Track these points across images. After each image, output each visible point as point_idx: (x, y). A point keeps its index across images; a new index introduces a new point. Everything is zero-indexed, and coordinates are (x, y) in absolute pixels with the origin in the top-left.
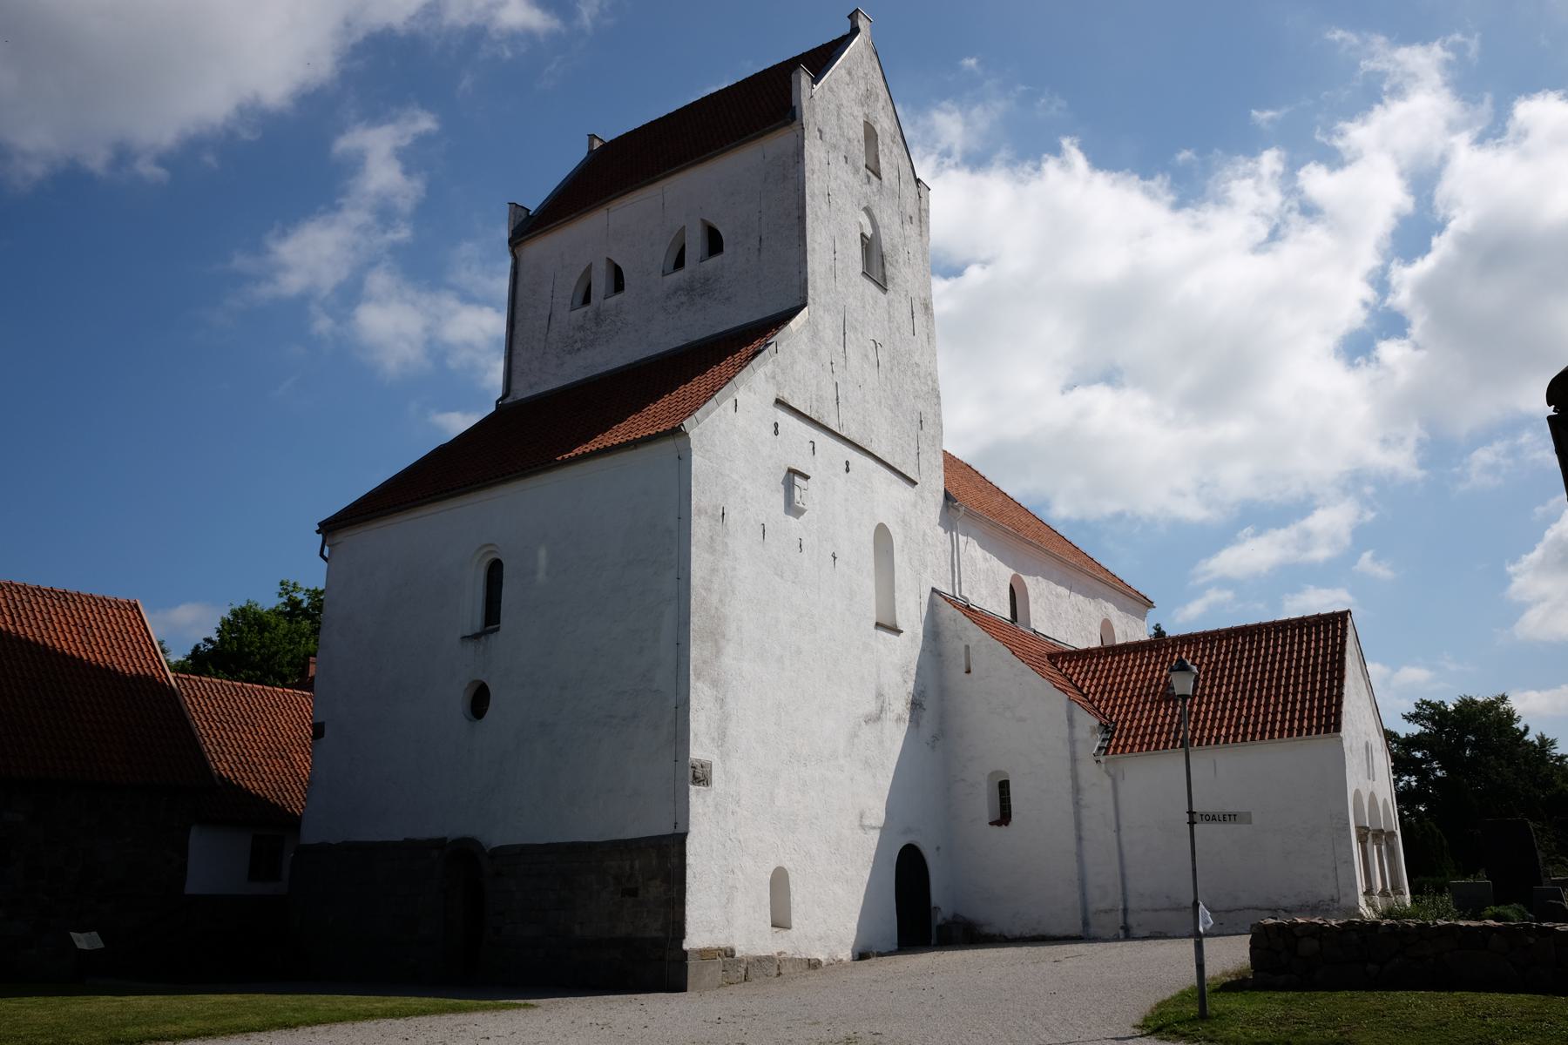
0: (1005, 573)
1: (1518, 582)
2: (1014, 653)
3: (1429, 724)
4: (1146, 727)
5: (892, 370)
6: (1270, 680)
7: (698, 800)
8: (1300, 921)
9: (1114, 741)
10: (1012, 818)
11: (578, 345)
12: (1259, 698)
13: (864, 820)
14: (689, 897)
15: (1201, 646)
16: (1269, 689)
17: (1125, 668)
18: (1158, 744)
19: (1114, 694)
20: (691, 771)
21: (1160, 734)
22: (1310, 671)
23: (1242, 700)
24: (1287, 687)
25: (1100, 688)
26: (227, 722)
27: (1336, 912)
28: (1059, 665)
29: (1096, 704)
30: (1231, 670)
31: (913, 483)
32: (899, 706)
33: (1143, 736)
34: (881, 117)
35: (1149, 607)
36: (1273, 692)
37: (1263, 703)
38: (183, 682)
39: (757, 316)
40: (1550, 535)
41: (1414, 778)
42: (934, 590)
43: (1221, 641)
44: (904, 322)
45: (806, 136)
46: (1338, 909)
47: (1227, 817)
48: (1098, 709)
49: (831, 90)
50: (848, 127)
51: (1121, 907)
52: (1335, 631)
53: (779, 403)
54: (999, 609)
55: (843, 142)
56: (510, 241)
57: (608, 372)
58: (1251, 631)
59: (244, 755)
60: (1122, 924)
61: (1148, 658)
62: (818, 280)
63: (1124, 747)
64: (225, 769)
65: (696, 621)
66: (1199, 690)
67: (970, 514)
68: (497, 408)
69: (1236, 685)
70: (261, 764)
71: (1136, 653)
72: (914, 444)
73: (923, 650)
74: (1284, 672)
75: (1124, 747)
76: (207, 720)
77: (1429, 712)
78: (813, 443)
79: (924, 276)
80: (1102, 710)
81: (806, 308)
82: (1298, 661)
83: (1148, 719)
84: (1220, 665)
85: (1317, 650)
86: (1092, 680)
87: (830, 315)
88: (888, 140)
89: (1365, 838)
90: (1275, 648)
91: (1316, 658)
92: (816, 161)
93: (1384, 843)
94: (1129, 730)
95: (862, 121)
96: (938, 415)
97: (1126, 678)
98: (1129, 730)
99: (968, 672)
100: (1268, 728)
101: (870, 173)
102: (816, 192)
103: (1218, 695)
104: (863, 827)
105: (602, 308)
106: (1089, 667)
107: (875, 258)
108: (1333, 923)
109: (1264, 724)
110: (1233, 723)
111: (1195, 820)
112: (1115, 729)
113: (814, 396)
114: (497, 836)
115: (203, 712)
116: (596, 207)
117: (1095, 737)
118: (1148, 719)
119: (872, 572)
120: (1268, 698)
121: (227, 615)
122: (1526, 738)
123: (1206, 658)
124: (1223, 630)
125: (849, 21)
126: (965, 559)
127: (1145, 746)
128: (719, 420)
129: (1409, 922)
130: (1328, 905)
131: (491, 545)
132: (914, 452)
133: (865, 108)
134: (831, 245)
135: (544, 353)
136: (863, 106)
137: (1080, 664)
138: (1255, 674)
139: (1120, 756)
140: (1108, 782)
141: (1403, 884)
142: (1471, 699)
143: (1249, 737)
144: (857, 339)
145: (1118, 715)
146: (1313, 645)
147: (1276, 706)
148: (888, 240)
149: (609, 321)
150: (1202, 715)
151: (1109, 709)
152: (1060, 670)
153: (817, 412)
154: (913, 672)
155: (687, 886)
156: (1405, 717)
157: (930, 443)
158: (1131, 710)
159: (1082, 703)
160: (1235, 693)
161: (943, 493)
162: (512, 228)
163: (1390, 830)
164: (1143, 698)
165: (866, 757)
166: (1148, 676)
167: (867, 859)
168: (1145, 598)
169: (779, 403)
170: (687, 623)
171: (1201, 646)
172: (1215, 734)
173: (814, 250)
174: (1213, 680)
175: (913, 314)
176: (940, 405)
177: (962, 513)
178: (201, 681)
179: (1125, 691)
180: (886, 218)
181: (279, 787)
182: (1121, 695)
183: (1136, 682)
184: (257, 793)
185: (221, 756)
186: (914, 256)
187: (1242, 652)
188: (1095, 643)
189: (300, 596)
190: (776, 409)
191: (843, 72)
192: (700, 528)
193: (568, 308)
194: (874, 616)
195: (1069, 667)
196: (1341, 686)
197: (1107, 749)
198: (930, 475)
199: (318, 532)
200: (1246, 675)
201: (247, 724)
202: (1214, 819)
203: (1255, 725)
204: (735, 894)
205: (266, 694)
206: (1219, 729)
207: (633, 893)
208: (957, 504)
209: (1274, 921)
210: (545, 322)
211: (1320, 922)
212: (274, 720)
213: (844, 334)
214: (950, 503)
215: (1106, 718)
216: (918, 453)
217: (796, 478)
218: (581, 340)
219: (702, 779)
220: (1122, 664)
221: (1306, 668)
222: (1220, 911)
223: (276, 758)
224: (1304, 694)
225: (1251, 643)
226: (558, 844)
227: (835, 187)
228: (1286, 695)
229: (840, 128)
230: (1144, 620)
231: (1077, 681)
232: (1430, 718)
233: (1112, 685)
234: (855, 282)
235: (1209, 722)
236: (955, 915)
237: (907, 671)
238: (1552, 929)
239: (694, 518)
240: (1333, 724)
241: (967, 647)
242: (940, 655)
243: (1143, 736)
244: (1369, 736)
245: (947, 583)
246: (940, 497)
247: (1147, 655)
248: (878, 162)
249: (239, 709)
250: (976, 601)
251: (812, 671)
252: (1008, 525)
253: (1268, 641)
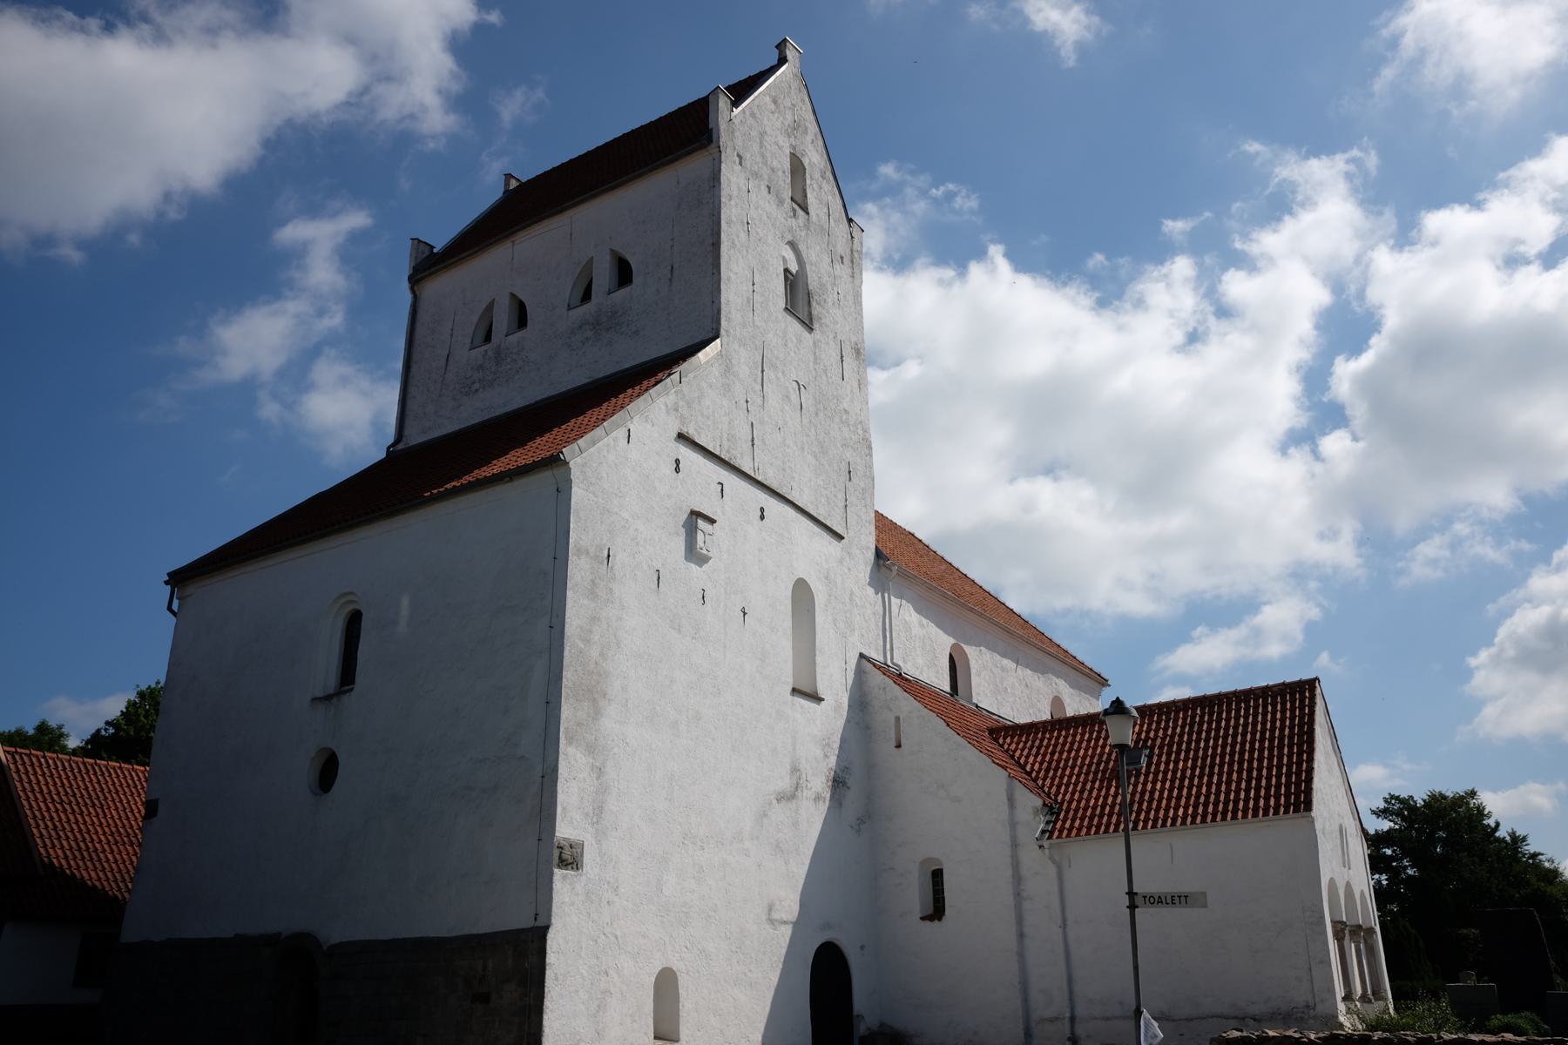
0: (945, 642)
1: (1479, 678)
2: (948, 725)
3: (1399, 820)
4: (1094, 808)
5: (817, 414)
6: (1232, 755)
7: (561, 880)
8: (1271, 1033)
9: (1060, 823)
10: (946, 913)
11: (477, 386)
12: (1220, 774)
13: (773, 913)
14: (548, 1003)
15: (1155, 719)
16: (1231, 764)
17: (1072, 744)
18: (1108, 826)
19: (1060, 771)
20: (556, 853)
21: (1110, 815)
22: (1276, 744)
23: (1201, 777)
24: (1250, 762)
25: (1045, 764)
26: (70, 803)
27: (1312, 1021)
28: (1001, 741)
29: (1040, 782)
30: (1189, 743)
31: (840, 537)
32: (819, 783)
33: (1091, 819)
34: (809, 150)
35: (1103, 685)
36: (1236, 768)
37: (1224, 779)
38: (22, 759)
39: (667, 351)
40: (1502, 632)
41: (1384, 877)
42: (862, 656)
43: (1177, 713)
44: (832, 365)
45: (723, 159)
46: (1315, 1017)
47: (1177, 899)
48: (1042, 788)
49: (753, 115)
50: (772, 157)
51: (1068, 1015)
52: (1302, 701)
53: (682, 437)
54: (937, 681)
55: (765, 172)
56: (410, 279)
57: (507, 414)
58: (1210, 701)
59: (84, 840)
60: (1069, 1035)
61: (1098, 732)
62: (733, 311)
63: (1070, 830)
64: (57, 857)
65: (569, 677)
66: (1153, 766)
67: (903, 575)
69: (1195, 760)
70: (104, 851)
71: (1084, 727)
72: (841, 496)
73: (848, 721)
74: (1248, 745)
75: (1070, 830)
76: (45, 801)
77: (1397, 807)
78: (722, 484)
79: (856, 319)
80: (1046, 790)
81: (718, 341)
82: (1263, 733)
83: (1097, 799)
84: (1176, 739)
85: (1283, 720)
86: (1036, 756)
87: (747, 350)
88: (817, 176)
89: (1341, 934)
90: (1237, 718)
91: (1282, 729)
92: (734, 187)
93: (1362, 941)
94: (1076, 811)
95: (788, 151)
96: (870, 466)
97: (1073, 753)
98: (1076, 811)
99: (899, 746)
100: (1230, 808)
101: (796, 207)
102: (734, 219)
103: (1175, 772)
104: (771, 921)
105: (502, 347)
106: (1034, 742)
107: (801, 296)
108: (1313, 1037)
109: (1226, 803)
110: (1192, 802)
111: (1136, 904)
112: (1060, 809)
113: (725, 436)
114: (335, 933)
115: (41, 792)
116: (499, 240)
117: (1037, 818)
118: (1097, 799)
119: (790, 631)
120: (1230, 774)
121: (133, 696)
122: (1497, 834)
123: (1161, 731)
124: (1179, 701)
125: (777, 51)
126: (898, 623)
127: (1094, 829)
128: (608, 451)
129: (1405, 1035)
130: (1303, 1012)
131: (351, 593)
132: (842, 505)
133: (792, 139)
134: (750, 276)
135: (440, 396)
136: (790, 137)
137: (1024, 739)
138: (1215, 748)
139: (1065, 840)
140: (1052, 870)
141: (1385, 991)
142: (1440, 794)
143: (1210, 817)
144: (778, 379)
145: (1064, 795)
146: (1279, 716)
147: (1239, 783)
148: (816, 278)
149: (509, 360)
150: (1157, 793)
151: (1054, 788)
152: (1002, 746)
153: (728, 452)
154: (836, 745)
155: (546, 990)
156: (1374, 812)
157: (860, 496)
158: (1079, 788)
159: (1024, 781)
160: (1193, 769)
161: (874, 551)
162: (413, 264)
163: (1368, 926)
164: (1091, 775)
165: (776, 841)
166: (1098, 752)
167: (776, 959)
168: (1099, 675)
169: (682, 437)
170: (560, 678)
171: (1155, 719)
172: (1171, 814)
173: (729, 279)
174: (1169, 755)
175: (842, 357)
176: (871, 456)
177: (895, 573)
178: (44, 757)
179: (1073, 768)
180: (813, 255)
181: (122, 877)
182: (1067, 772)
183: (1084, 758)
184: (94, 885)
185: (56, 842)
186: (845, 297)
187: (1201, 724)
188: (1046, 716)
190: (677, 444)
191: (768, 99)
192: (579, 570)
193: (468, 346)
194: (790, 680)
195: (1012, 742)
196: (1311, 760)
197: (1052, 833)
198: (859, 530)
199: (166, 583)
200: (1206, 749)
201: (94, 805)
202: (1160, 902)
203: (1216, 804)
204: (609, 1000)
205: (123, 773)
206: (1176, 809)
207: (485, 998)
208: (888, 562)
209: (1238, 1034)
210: (443, 362)
211: (1297, 1035)
212: (128, 802)
213: (763, 371)
214: (882, 562)
215: (1051, 798)
216: (846, 506)
217: (699, 521)
218: (480, 380)
219: (570, 861)
220: (1069, 739)
221: (1271, 740)
222: (1180, 1020)
223: (124, 844)
224: (1269, 769)
225: (1211, 715)
226: (405, 940)
227: (755, 216)
228: (1250, 771)
229: (763, 156)
230: (1098, 699)
231: (1019, 758)
232: (1399, 814)
233: (1058, 761)
234: (777, 318)
235: (1164, 802)
236: (882, 1025)
237: (828, 745)
238: (1515, 1035)
239: (572, 558)
240: (1303, 802)
241: (897, 719)
242: (868, 728)
243: (1091, 819)
244: (1343, 818)
245: (877, 650)
246: (871, 555)
247: (1096, 729)
248: (806, 196)
249: (87, 789)
250: (910, 669)
251: (713, 739)
252: (948, 590)
253: (1229, 712)
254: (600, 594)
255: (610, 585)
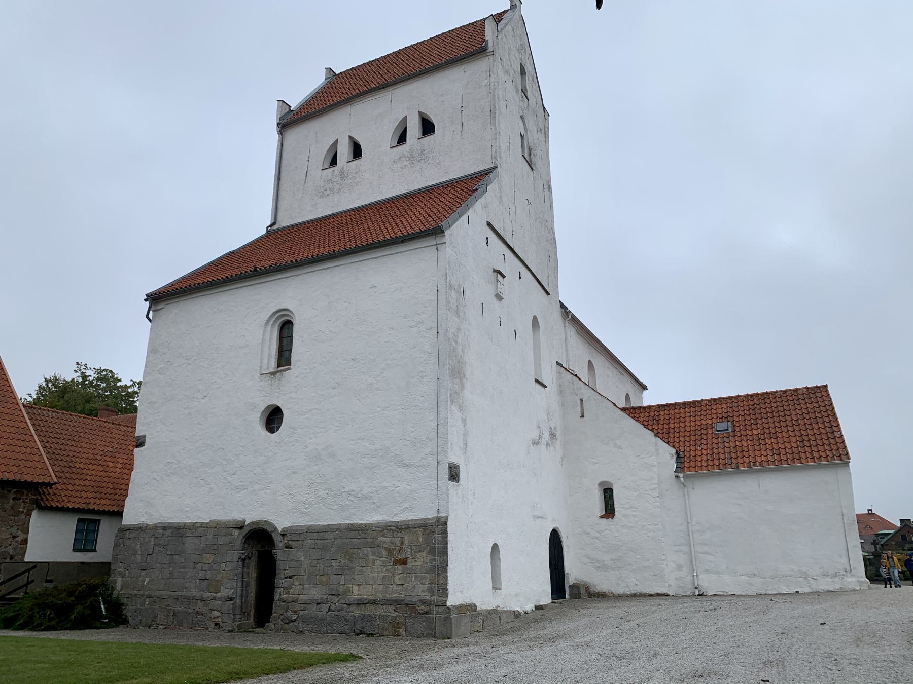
11: (328, 192)
68: (267, 232)
149: (350, 177)
189: (88, 373)
199: (146, 300)
242: (563, 405)
254: (460, 314)
255: (464, 309)
